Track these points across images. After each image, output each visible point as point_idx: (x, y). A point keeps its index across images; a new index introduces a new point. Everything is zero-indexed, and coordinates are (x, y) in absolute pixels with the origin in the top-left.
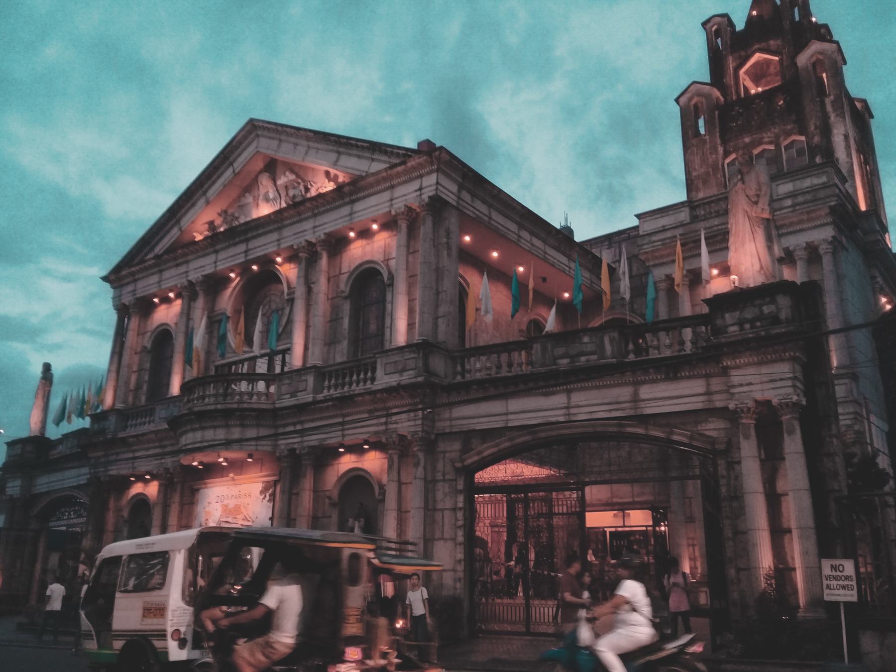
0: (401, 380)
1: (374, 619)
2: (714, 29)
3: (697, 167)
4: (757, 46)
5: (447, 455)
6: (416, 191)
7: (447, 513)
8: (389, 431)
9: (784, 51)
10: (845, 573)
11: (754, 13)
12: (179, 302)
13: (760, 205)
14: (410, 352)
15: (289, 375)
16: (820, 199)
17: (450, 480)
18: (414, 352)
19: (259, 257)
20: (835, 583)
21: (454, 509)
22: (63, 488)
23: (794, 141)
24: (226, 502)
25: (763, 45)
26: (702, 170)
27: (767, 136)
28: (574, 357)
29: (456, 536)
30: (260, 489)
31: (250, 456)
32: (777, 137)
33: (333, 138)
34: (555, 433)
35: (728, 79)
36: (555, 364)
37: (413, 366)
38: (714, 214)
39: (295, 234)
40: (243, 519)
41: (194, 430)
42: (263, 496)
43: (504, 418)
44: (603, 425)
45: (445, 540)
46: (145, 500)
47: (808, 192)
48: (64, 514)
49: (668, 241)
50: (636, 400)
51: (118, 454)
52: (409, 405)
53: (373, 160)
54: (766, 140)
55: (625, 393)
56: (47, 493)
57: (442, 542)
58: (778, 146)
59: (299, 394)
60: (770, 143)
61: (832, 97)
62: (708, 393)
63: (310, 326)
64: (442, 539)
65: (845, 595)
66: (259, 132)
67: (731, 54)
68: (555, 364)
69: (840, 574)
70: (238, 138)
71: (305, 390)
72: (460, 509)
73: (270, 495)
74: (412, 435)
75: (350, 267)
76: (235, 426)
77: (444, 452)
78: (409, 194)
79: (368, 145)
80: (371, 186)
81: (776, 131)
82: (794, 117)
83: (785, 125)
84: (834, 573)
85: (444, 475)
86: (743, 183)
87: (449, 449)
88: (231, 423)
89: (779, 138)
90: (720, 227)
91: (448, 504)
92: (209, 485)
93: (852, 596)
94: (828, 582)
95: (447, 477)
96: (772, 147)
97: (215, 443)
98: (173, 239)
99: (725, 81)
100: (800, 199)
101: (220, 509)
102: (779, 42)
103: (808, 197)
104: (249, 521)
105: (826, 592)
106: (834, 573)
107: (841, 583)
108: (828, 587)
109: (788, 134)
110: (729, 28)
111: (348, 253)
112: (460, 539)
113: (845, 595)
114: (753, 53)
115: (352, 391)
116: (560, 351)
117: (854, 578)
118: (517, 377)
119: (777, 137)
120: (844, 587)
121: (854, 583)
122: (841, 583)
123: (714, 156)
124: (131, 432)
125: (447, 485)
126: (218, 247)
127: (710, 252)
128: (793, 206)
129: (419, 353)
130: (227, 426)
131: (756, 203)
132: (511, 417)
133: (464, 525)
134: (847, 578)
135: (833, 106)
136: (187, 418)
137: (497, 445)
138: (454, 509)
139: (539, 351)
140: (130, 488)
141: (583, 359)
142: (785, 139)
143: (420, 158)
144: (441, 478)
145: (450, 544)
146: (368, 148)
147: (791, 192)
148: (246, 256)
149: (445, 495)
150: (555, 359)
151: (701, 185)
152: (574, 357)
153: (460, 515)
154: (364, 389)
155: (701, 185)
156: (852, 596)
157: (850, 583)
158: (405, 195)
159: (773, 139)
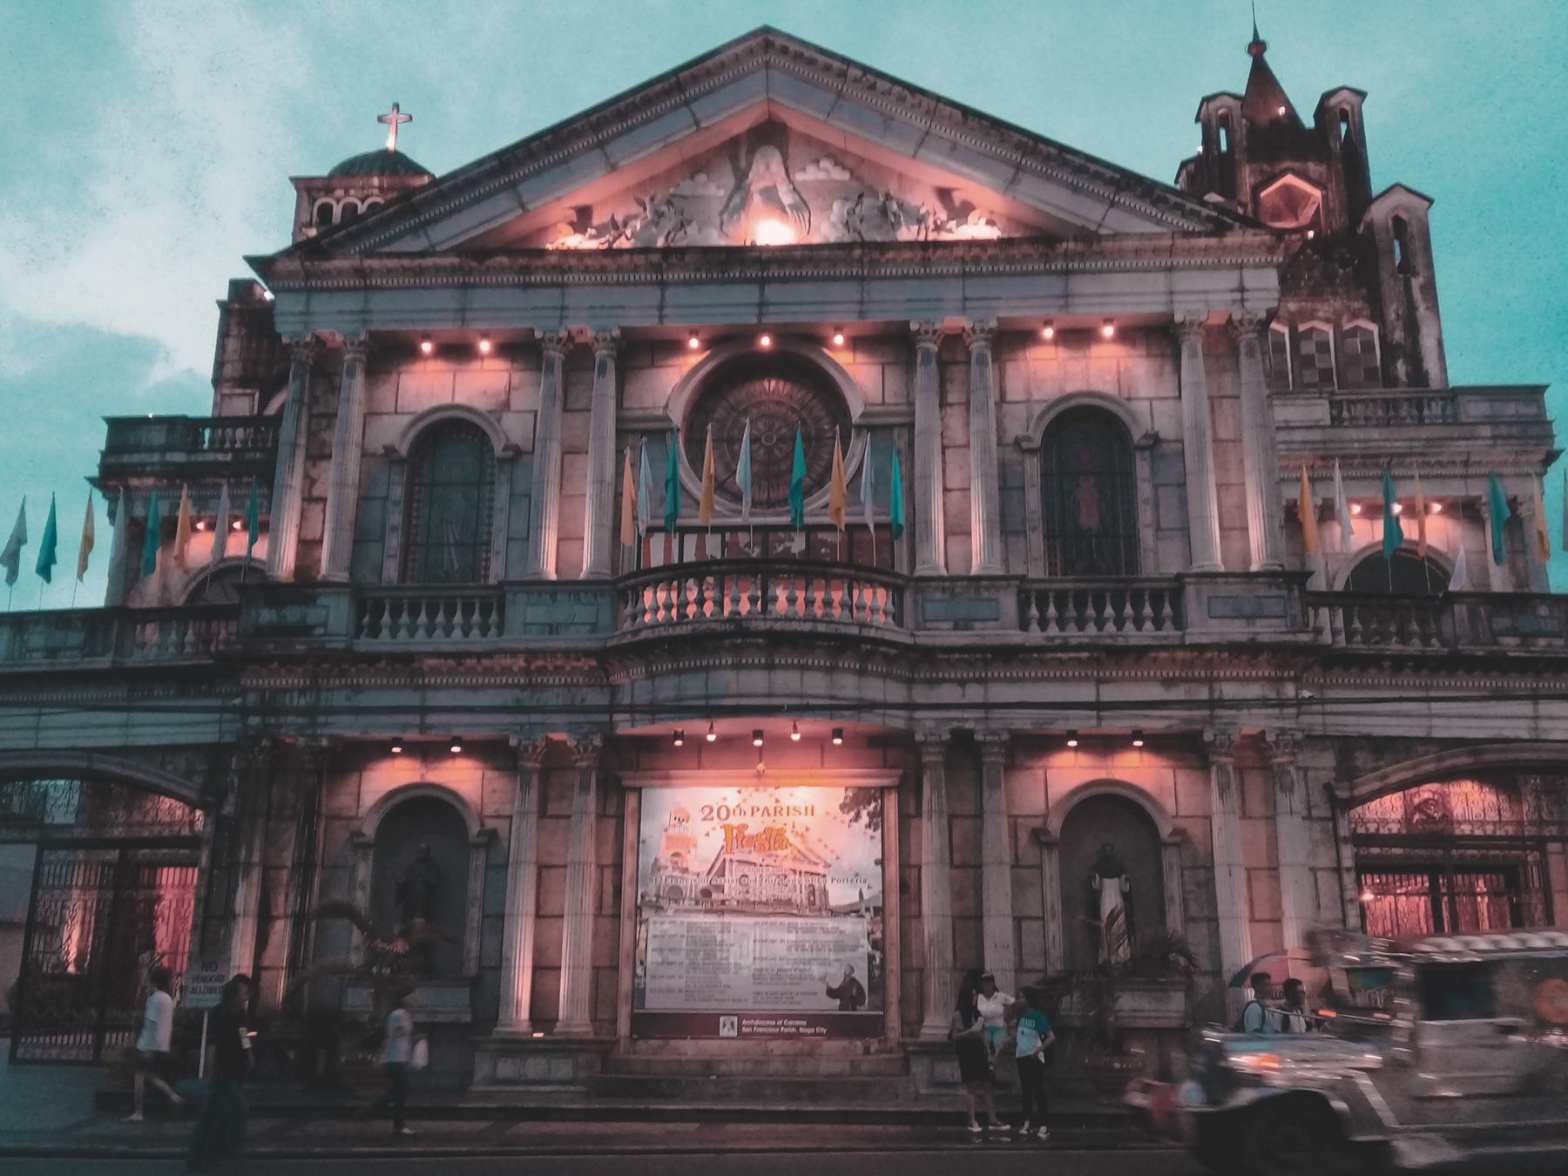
0: (1259, 634)
2: (1220, 112)
4: (1287, 164)
6: (1232, 291)
8: (1217, 721)
9: (1329, 185)
11: (1282, 111)
14: (1270, 585)
15: (947, 584)
16: (1532, 438)
17: (1322, 819)
18: (1279, 587)
19: (776, 325)
22: (36, 749)
23: (1357, 328)
24: (734, 821)
25: (1297, 165)
27: (1324, 309)
28: (1526, 638)
30: (842, 800)
33: (1017, 137)
34: (1511, 756)
36: (1496, 643)
37: (1278, 610)
38: (1362, 422)
39: (910, 301)
40: (795, 859)
41: (886, 676)
42: (852, 814)
43: (1424, 721)
44: (1559, 751)
47: (1516, 423)
49: (1295, 446)
51: (358, 689)
53: (1112, 204)
54: (1321, 314)
59: (978, 625)
66: (773, 58)
67: (1249, 161)
68: (1496, 643)
70: (723, 57)
71: (997, 620)
73: (871, 816)
74: (1278, 735)
76: (849, 670)
78: (1215, 291)
79: (1118, 176)
80: (1121, 253)
82: (1364, 291)
87: (1313, 763)
88: (844, 663)
90: (1382, 444)
92: (674, 782)
95: (1315, 813)
97: (745, 702)
98: (493, 225)
100: (1503, 430)
101: (718, 838)
102: (1322, 168)
103: (1515, 430)
104: (815, 864)
109: (1355, 315)
111: (1022, 365)
114: (1283, 173)
115: (1124, 637)
116: (1502, 622)
124: (384, 642)
126: (669, 276)
127: (1344, 479)
128: (1494, 438)
129: (1290, 590)
130: (831, 670)
132: (1435, 721)
136: (957, 656)
137: (1414, 767)
139: (1466, 619)
140: (366, 770)
141: (1542, 642)
143: (1255, 235)
146: (1111, 182)
147: (1486, 417)
148: (761, 315)
150: (1495, 635)
152: (1526, 638)
154: (1154, 638)
158: (1206, 292)
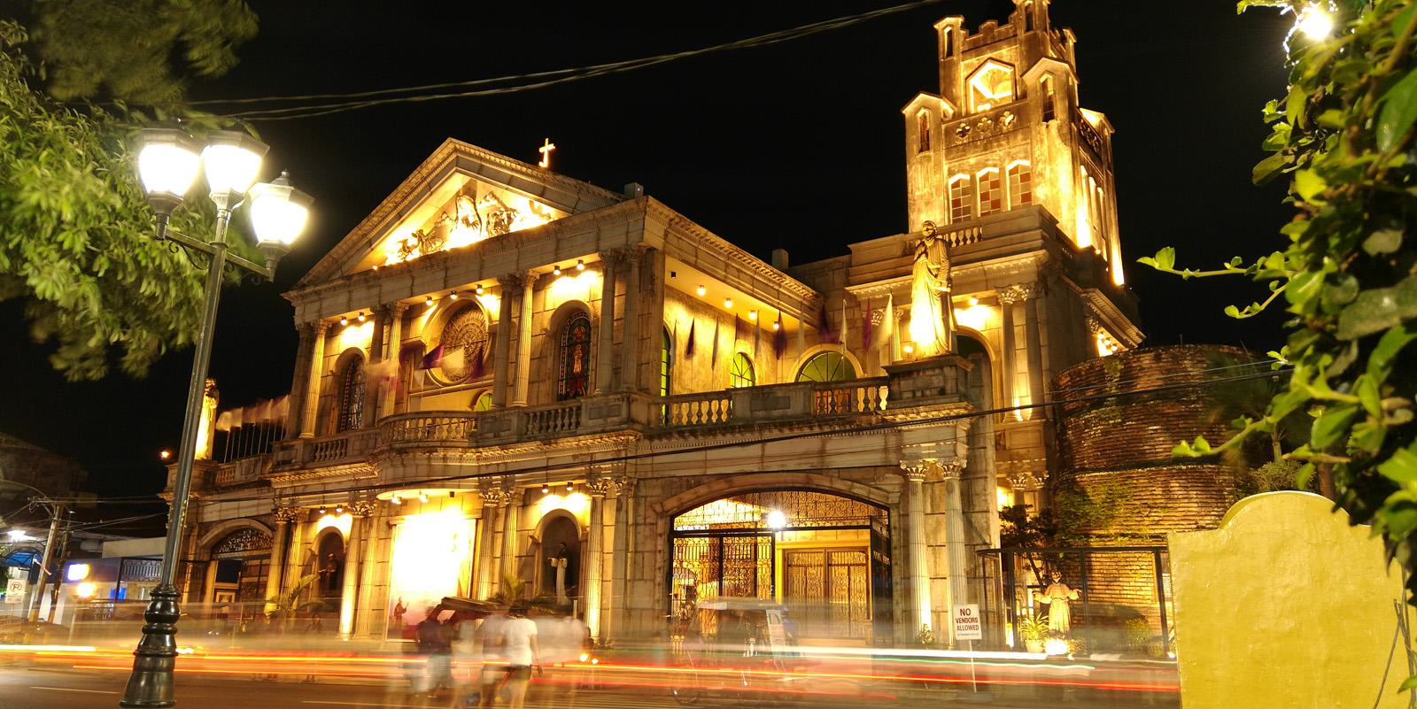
3: (920, 186)
5: (648, 499)
7: (646, 555)
10: (971, 616)
13: (939, 279)
20: (964, 624)
21: (655, 552)
26: (926, 190)
29: (655, 576)
35: (958, 87)
45: (646, 581)
46: (337, 535)
48: (238, 546)
50: (822, 453)
54: (990, 162)
55: (813, 444)
56: (217, 522)
57: (642, 582)
60: (995, 166)
62: (886, 450)
64: (642, 579)
65: (973, 634)
69: (968, 617)
72: (660, 551)
75: (554, 304)
77: (646, 497)
81: (1001, 153)
84: (963, 617)
85: (645, 519)
86: (927, 256)
91: (649, 546)
93: (978, 634)
94: (959, 624)
95: (648, 521)
99: (954, 91)
106: (963, 617)
107: (968, 624)
112: (659, 579)
113: (973, 634)
117: (979, 620)
119: (1002, 160)
120: (970, 628)
121: (979, 624)
122: (968, 624)
123: (938, 176)
125: (648, 528)
131: (936, 276)
134: (973, 620)
138: (655, 552)
142: (1009, 163)
144: (642, 521)
145: (649, 584)
149: (646, 537)
151: (923, 206)
153: (659, 557)
155: (923, 206)
156: (978, 634)
157: (975, 624)
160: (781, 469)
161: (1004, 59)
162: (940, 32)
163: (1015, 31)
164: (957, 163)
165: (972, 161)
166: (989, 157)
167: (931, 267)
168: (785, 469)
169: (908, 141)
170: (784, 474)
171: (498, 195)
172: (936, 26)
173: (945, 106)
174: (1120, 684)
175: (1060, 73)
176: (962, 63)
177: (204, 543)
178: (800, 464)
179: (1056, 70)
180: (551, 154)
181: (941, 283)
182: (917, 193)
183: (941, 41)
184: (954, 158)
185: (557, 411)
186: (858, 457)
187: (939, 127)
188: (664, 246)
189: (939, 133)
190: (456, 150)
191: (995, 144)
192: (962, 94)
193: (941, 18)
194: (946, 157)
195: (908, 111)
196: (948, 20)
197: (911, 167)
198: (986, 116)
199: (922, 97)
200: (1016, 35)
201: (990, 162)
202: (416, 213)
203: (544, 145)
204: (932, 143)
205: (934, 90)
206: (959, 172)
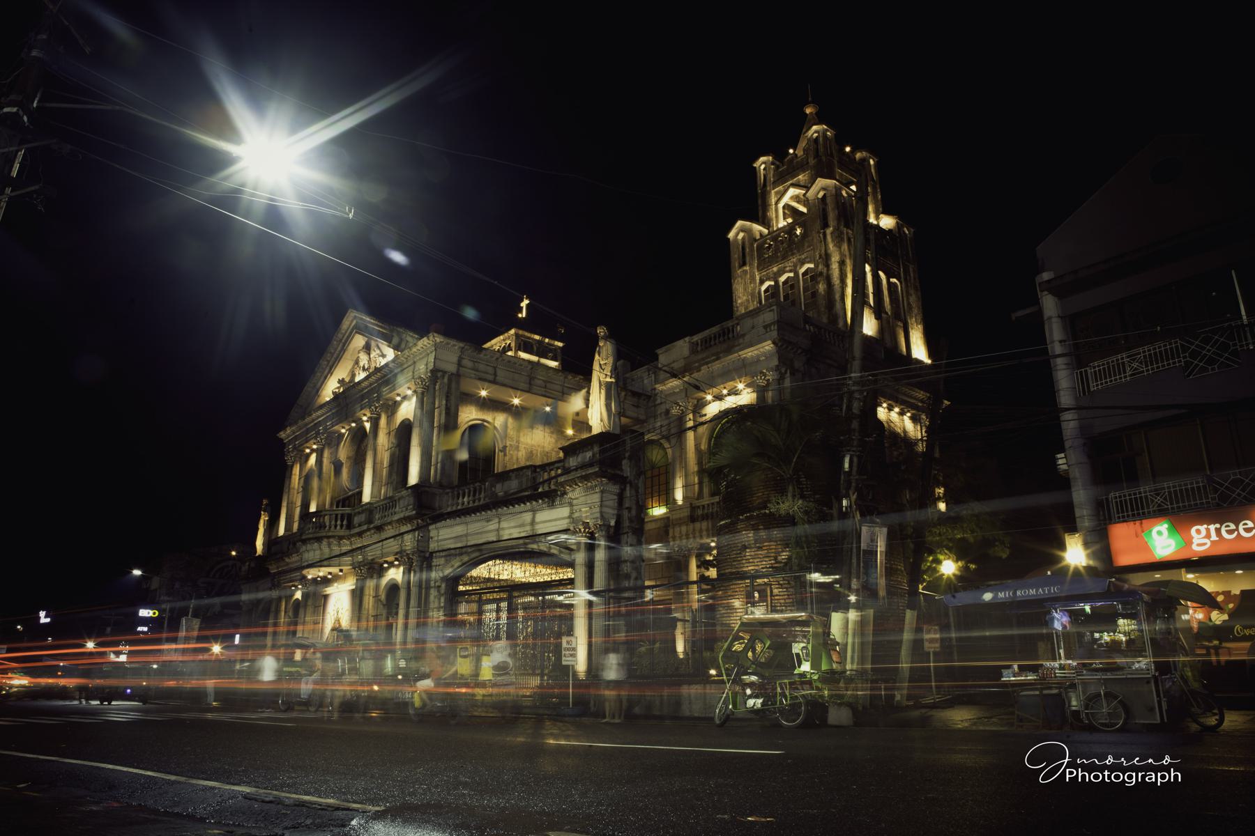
1: (400, 586)
12: (414, 399)
26: (745, 298)
31: (397, 559)
32: (795, 266)
52: (724, 617)
54: (788, 269)
58: (796, 273)
60: (790, 271)
61: (831, 229)
63: (839, 262)
83: (800, 255)
84: (568, 646)
89: (796, 267)
96: (792, 275)
105: (563, 658)
108: (565, 656)
110: (772, 166)
118: (460, 510)
119: (795, 266)
123: (752, 285)
133: (445, 593)
135: (832, 237)
159: (793, 268)
160: (509, 538)
161: (802, 183)
162: (757, 169)
163: (808, 160)
164: (765, 273)
165: (775, 269)
166: (787, 265)
167: (602, 363)
168: (512, 537)
169: (732, 260)
170: (513, 541)
171: (381, 348)
172: (755, 165)
173: (757, 228)
174: (159, 651)
175: (831, 189)
176: (773, 192)
177: (1163, 702)
178: (520, 532)
179: (828, 187)
180: (528, 306)
181: (606, 375)
182: (739, 301)
183: (758, 175)
184: (763, 269)
185: (337, 507)
186: (554, 523)
187: (752, 245)
188: (458, 369)
189: (752, 250)
190: (355, 317)
191: (790, 253)
192: (774, 216)
193: (757, 158)
194: (758, 269)
195: (731, 235)
196: (762, 159)
197: (734, 281)
198: (783, 232)
199: (739, 223)
200: (808, 163)
201: (788, 269)
202: (338, 367)
203: (523, 301)
204: (748, 259)
205: (754, 219)
206: (766, 280)
